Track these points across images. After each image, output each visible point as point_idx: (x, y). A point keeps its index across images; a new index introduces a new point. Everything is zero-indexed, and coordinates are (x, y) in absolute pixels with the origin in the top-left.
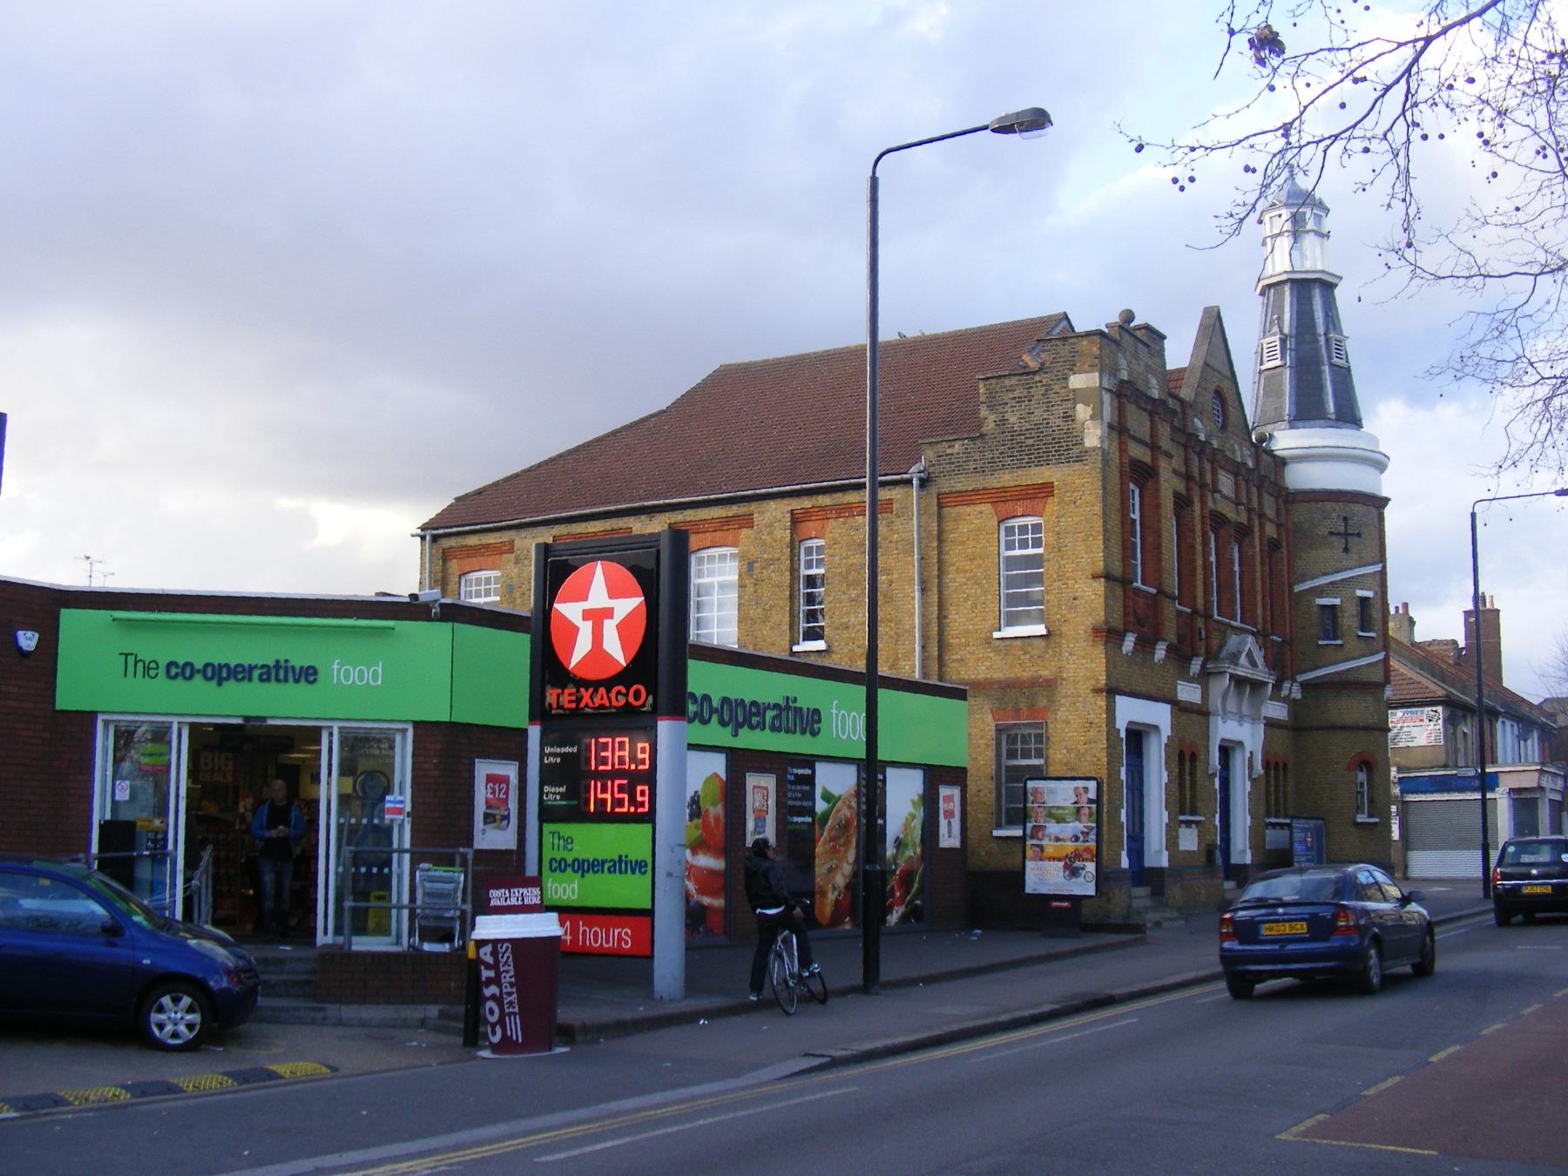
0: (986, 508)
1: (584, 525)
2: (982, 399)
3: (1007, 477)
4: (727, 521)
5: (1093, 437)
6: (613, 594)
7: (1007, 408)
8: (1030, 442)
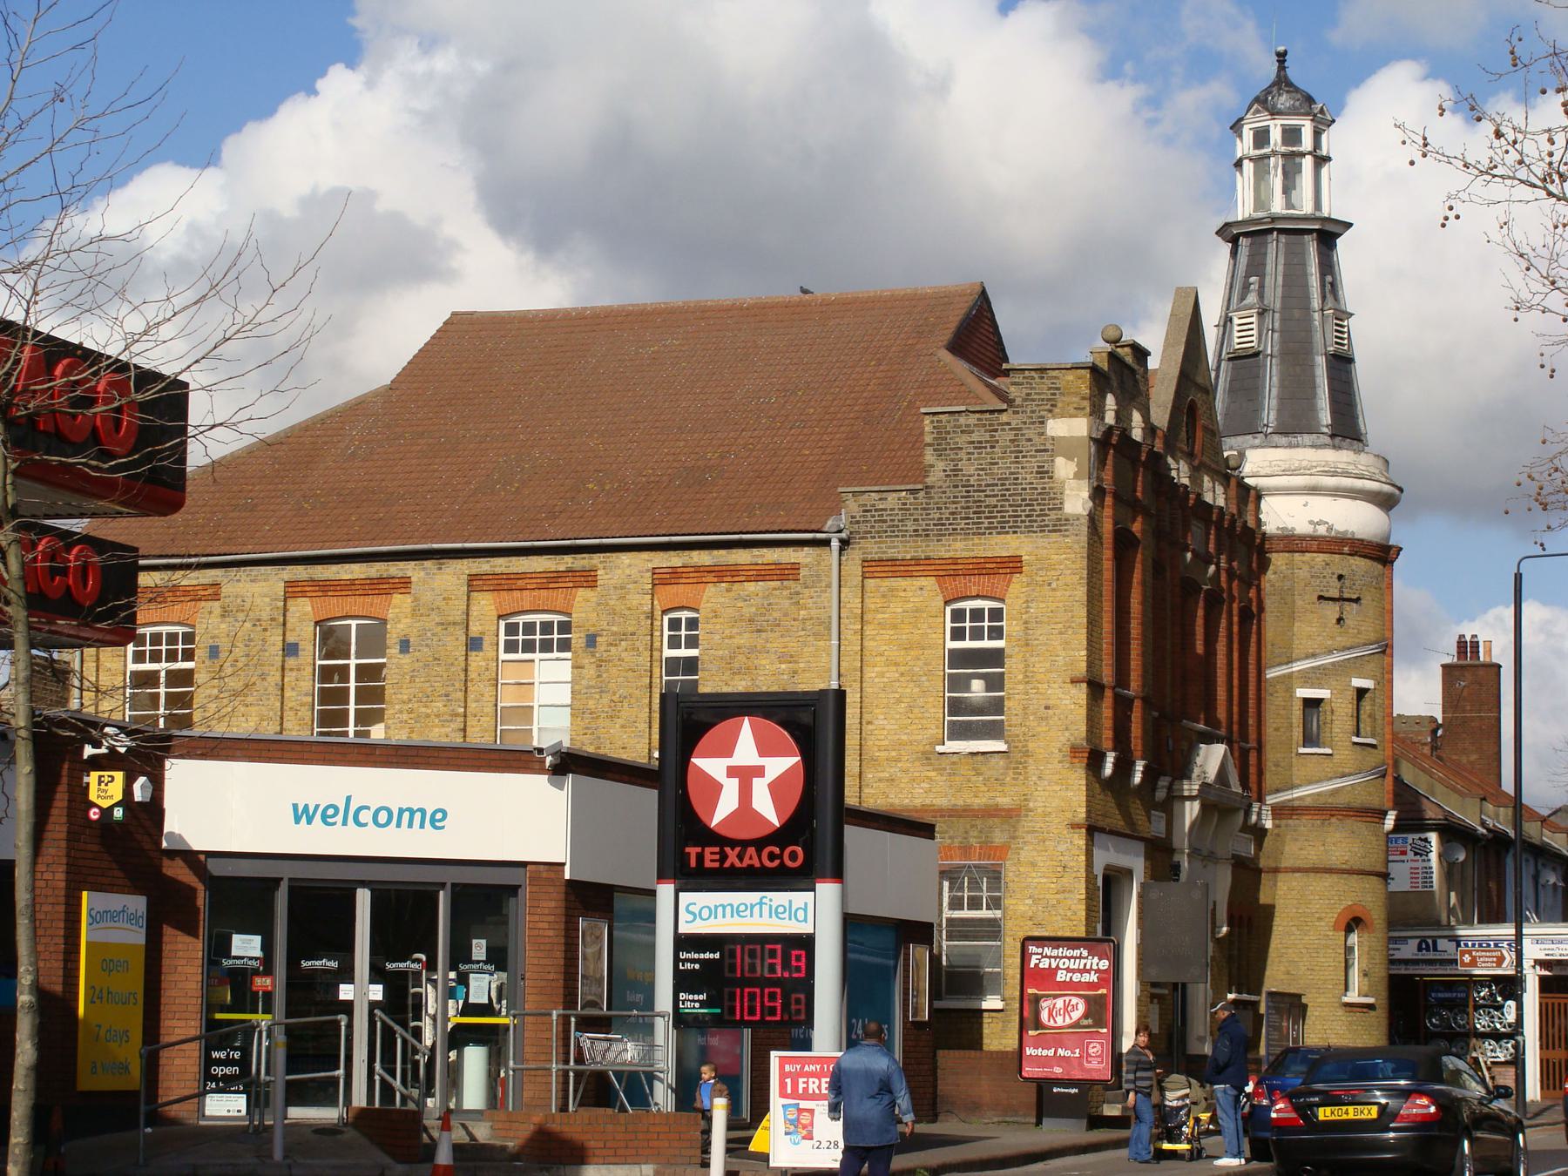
0: (929, 583)
1: (334, 568)
2: (928, 439)
3: (959, 545)
4: (554, 578)
5: (1077, 501)
6: (764, 751)
7: (962, 454)
8: (993, 501)
